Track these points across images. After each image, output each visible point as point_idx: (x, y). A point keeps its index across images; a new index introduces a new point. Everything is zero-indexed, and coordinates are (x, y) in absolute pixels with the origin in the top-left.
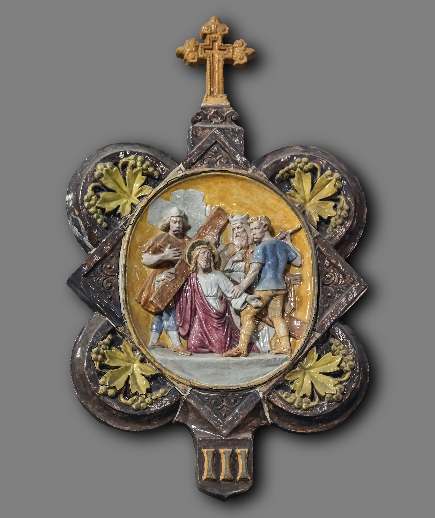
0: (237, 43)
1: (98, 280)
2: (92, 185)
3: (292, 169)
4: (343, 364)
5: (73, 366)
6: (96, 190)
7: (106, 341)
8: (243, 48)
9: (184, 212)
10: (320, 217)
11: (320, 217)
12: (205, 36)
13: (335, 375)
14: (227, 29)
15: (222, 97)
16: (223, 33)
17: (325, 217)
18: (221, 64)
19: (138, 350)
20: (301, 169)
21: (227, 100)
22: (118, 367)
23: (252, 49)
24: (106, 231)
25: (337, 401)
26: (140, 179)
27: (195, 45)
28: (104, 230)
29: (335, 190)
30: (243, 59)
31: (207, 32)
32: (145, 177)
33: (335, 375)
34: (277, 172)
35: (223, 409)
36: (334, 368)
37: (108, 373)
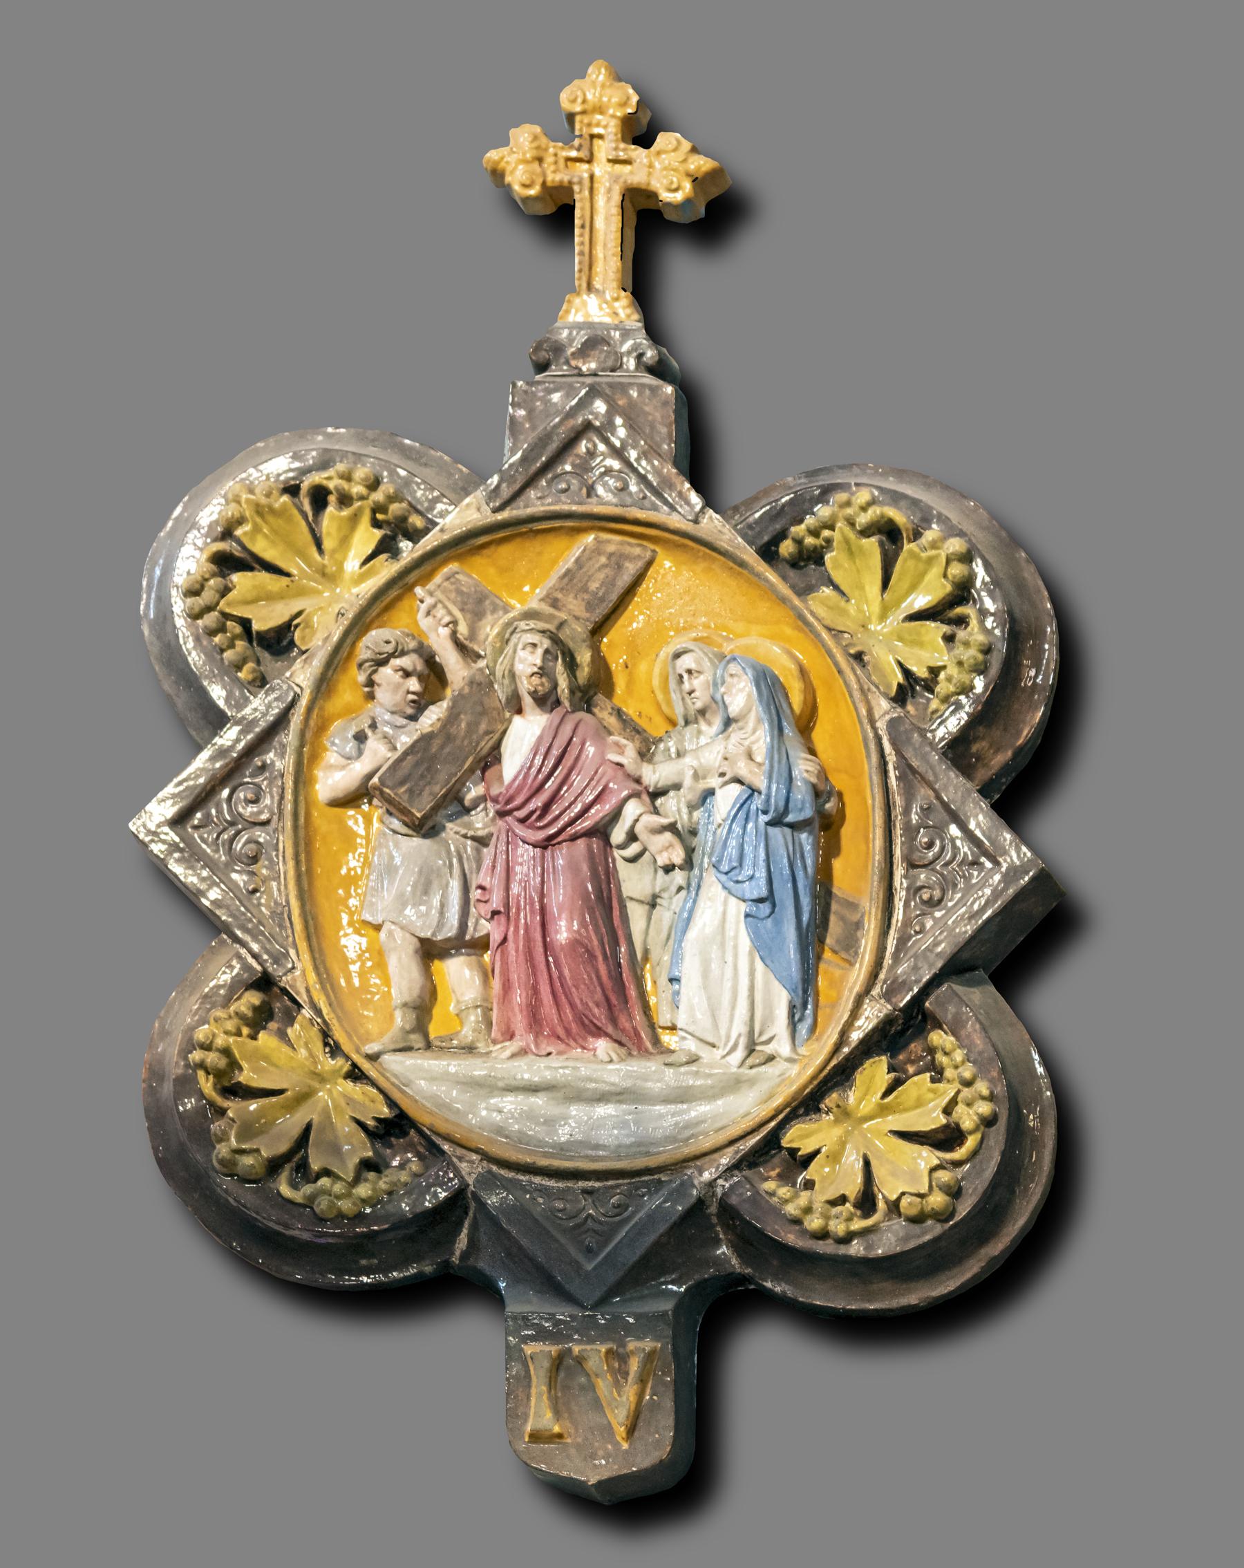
1: (969, 836)
4: (960, 1109)
5: (151, 1092)
8: (680, 155)
13: (946, 1138)
14: (635, 98)
17: (921, 672)
18: (617, 198)
19: (540, 1218)
20: (852, 524)
22: (280, 1092)
25: (941, 1216)
26: (366, 538)
30: (676, 190)
35: (586, 1227)
36: (932, 1119)
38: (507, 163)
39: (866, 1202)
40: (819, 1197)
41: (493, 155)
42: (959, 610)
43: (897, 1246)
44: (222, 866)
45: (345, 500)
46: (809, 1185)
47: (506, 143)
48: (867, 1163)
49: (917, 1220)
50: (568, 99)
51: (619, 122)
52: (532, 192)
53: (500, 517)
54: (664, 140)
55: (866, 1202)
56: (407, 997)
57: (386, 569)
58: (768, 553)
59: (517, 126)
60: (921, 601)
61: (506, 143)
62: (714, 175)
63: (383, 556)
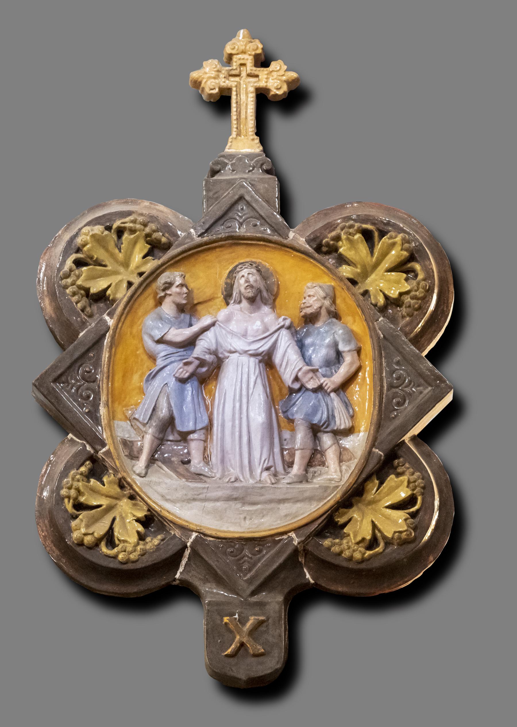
2: (74, 256)
7: (83, 469)
10: (386, 297)
11: (386, 297)
14: (260, 46)
15: (253, 140)
21: (259, 145)
23: (295, 73)
26: (142, 248)
27: (215, 69)
31: (233, 52)
34: (210, 437)
37: (83, 515)
38: (203, 78)
41: (195, 75)
43: (290, 459)
44: (410, 319)
45: (132, 231)
53: (206, 239)
54: (274, 65)
62: (295, 81)
63: (149, 258)
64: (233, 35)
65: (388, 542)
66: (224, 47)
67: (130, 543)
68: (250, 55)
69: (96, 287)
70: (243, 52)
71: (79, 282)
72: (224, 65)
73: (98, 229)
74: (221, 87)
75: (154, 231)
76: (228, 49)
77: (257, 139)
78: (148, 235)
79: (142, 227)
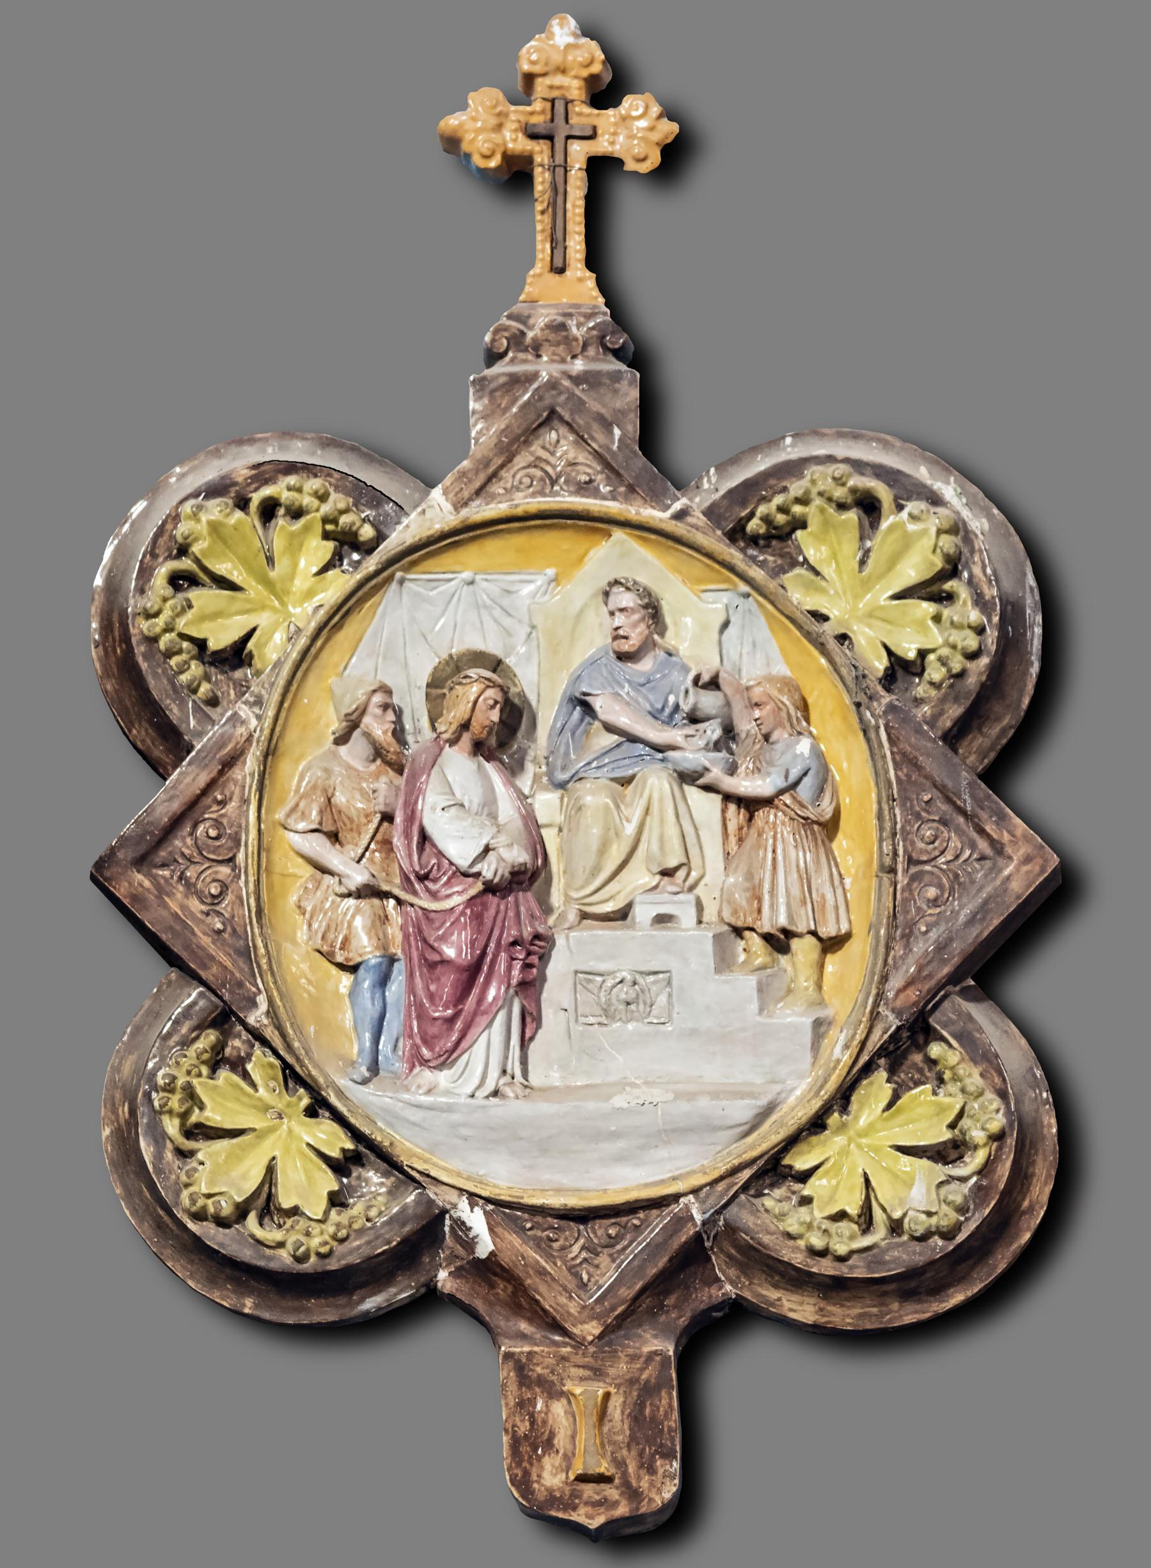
0: (632, 104)
3: (798, 501)
4: (965, 1123)
6: (178, 581)
9: (533, 746)
12: (529, 79)
13: (944, 1154)
16: (585, 73)
24: (207, 709)
28: (202, 706)
29: (939, 563)
31: (537, 69)
32: (330, 545)
33: (944, 1154)
39: (866, 1221)
40: (819, 1212)
41: (453, 121)
42: (948, 586)
46: (806, 1201)
47: (464, 107)
48: (867, 1181)
49: (923, 1238)
50: (530, 56)
51: (582, 83)
52: (493, 164)
55: (866, 1221)
56: (700, 706)
57: (339, 584)
58: (736, 534)
59: (476, 90)
60: (911, 572)
61: (464, 107)
64: (542, 27)
65: (896, 1227)
66: (516, 58)
67: (965, 1104)
68: (576, 77)
69: (220, 638)
70: (563, 71)
71: (181, 624)
72: (514, 102)
73: (215, 509)
74: (509, 153)
75: (342, 512)
76: (530, 56)
77: (589, 278)
78: (325, 520)
79: (316, 502)
